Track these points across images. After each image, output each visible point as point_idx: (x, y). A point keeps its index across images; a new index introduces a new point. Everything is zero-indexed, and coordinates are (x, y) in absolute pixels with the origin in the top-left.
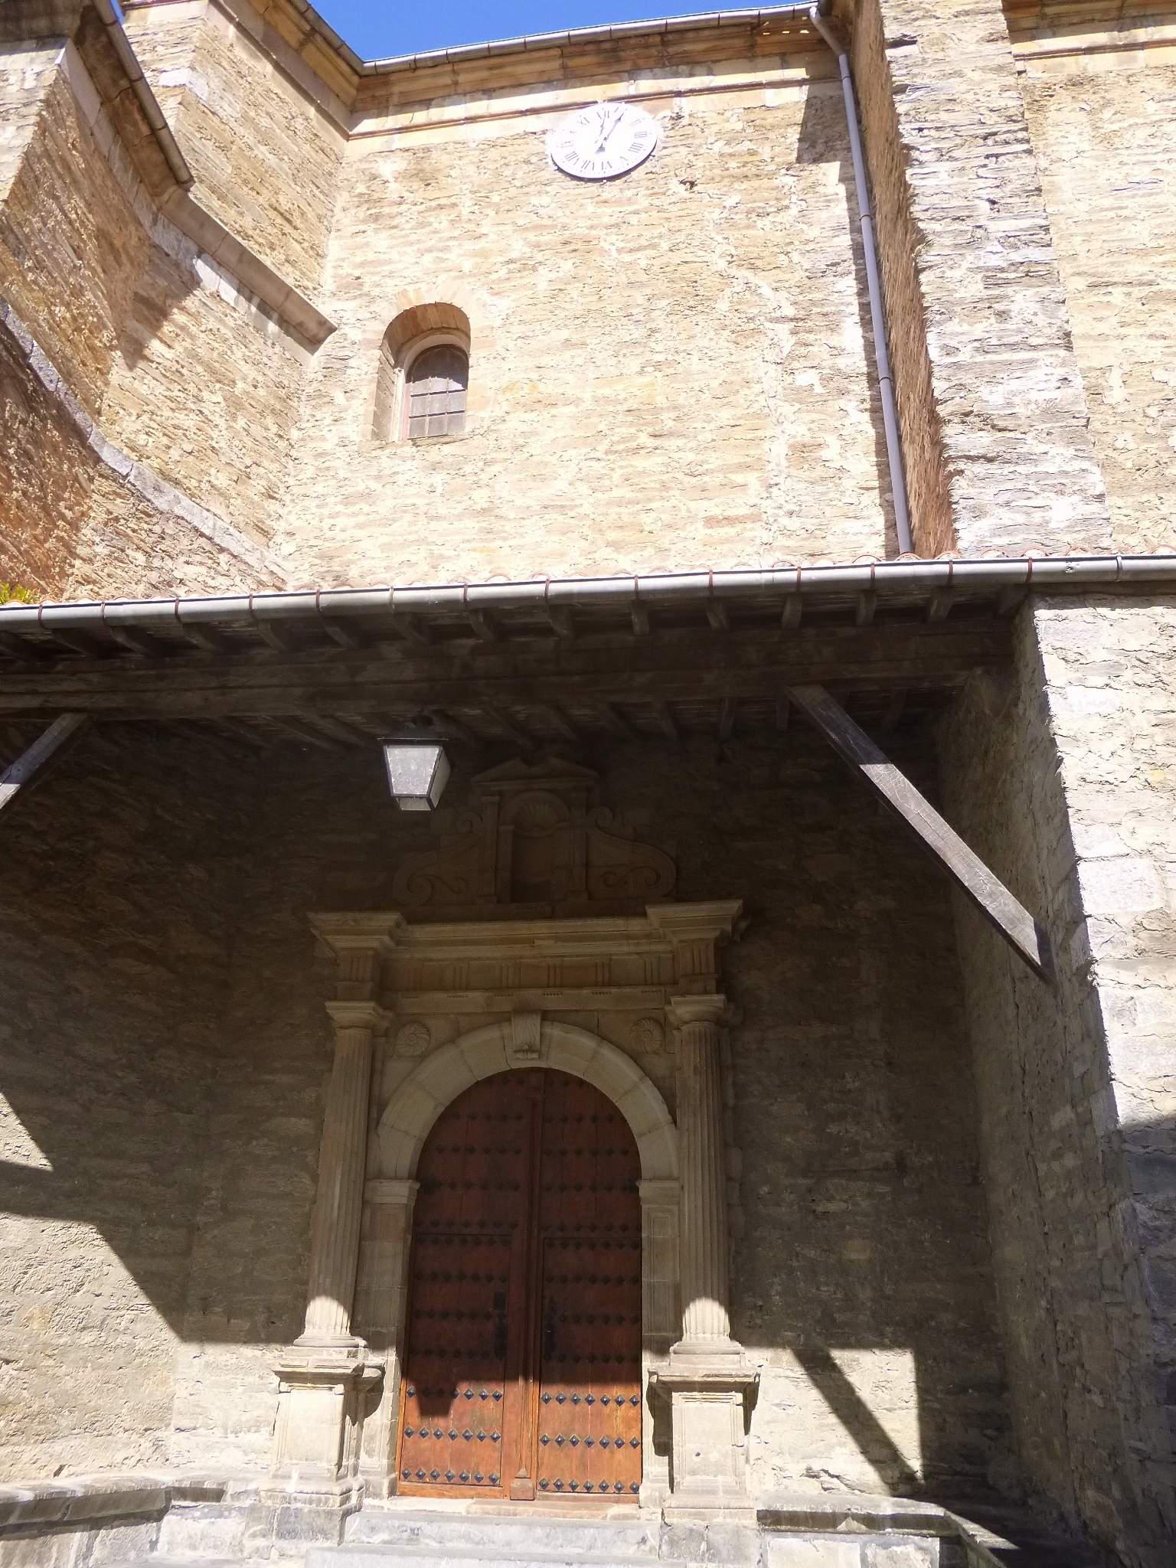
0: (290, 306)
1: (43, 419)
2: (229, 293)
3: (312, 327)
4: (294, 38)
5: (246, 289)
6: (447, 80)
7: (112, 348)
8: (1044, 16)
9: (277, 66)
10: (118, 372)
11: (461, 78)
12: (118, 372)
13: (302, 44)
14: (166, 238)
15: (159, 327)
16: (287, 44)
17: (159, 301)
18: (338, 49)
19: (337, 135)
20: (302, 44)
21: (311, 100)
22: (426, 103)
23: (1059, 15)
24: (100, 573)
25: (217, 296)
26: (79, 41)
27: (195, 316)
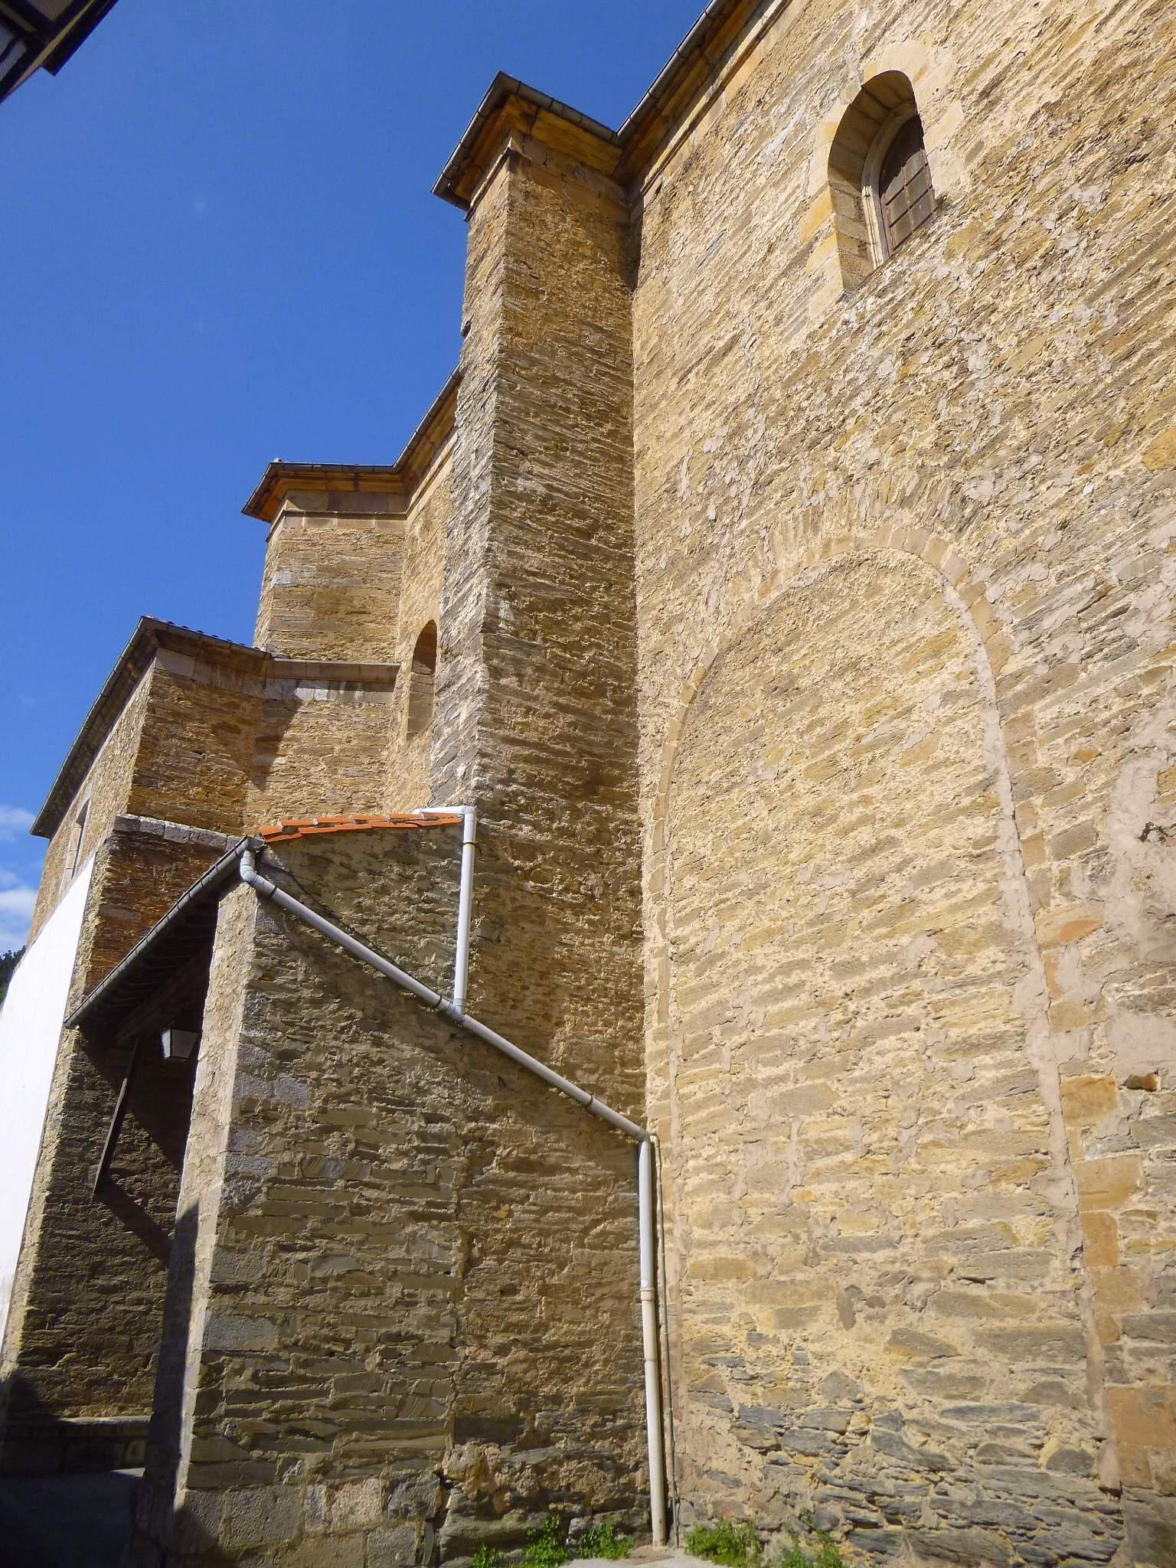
0: (365, 674)
1: (185, 860)
2: (321, 694)
3: (385, 675)
4: (349, 486)
5: (333, 684)
6: (428, 446)
7: (244, 782)
8: (666, 119)
9: (341, 516)
10: (252, 793)
11: (432, 439)
12: (252, 793)
13: (356, 485)
14: (272, 692)
15: (277, 749)
16: (347, 492)
17: (272, 734)
18: (374, 471)
19: (396, 522)
20: (356, 485)
21: (369, 516)
22: (429, 466)
23: (675, 108)
24: (847, 633)
25: (314, 702)
26: (163, 645)
27: (300, 726)
